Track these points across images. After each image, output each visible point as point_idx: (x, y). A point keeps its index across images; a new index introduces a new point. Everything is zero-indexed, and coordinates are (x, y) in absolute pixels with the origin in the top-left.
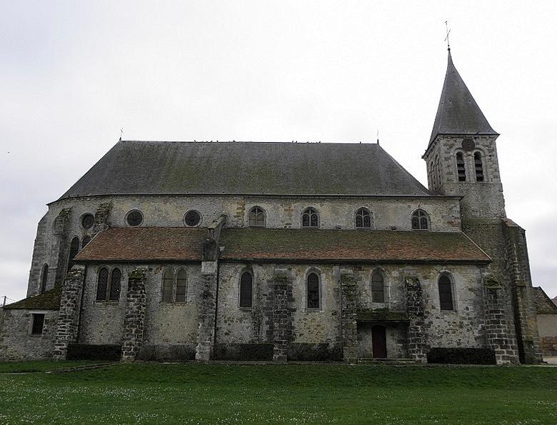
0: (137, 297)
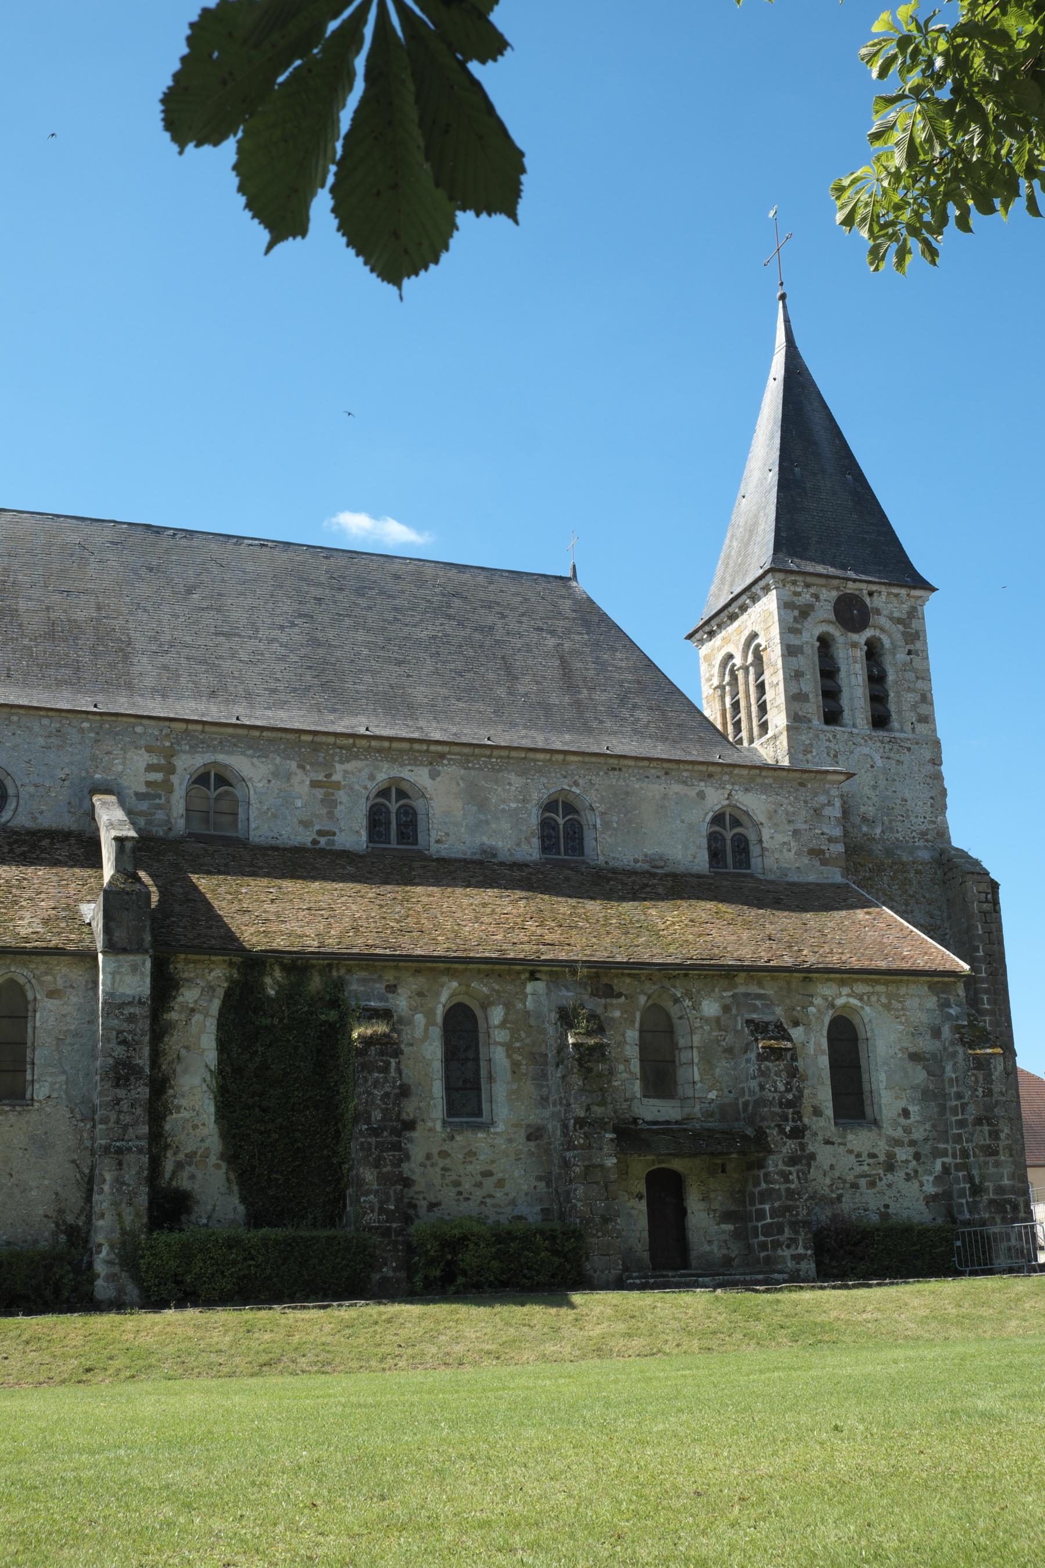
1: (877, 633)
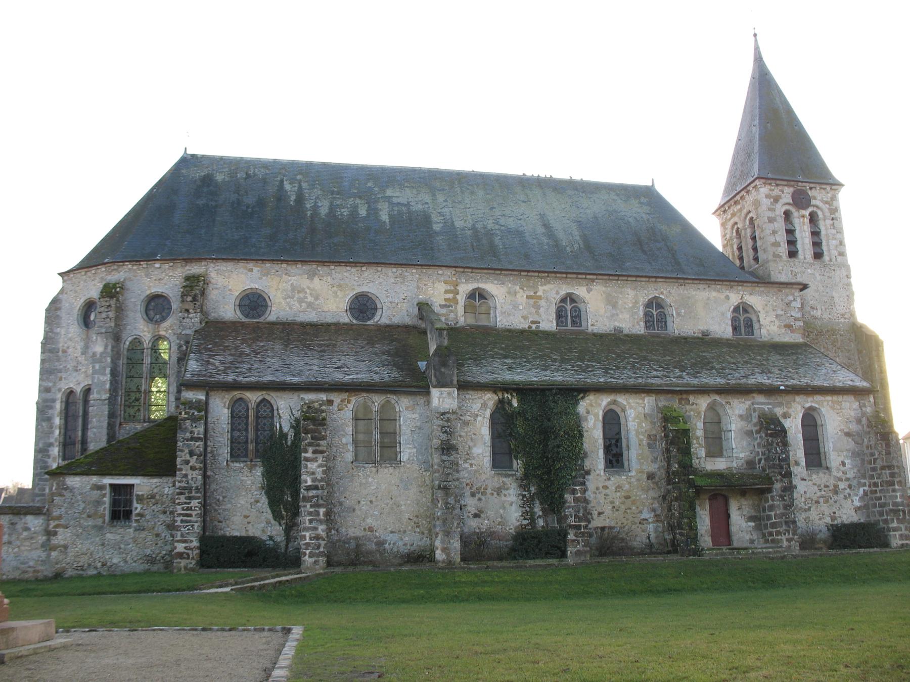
0: (322, 452)
1: (815, 209)
